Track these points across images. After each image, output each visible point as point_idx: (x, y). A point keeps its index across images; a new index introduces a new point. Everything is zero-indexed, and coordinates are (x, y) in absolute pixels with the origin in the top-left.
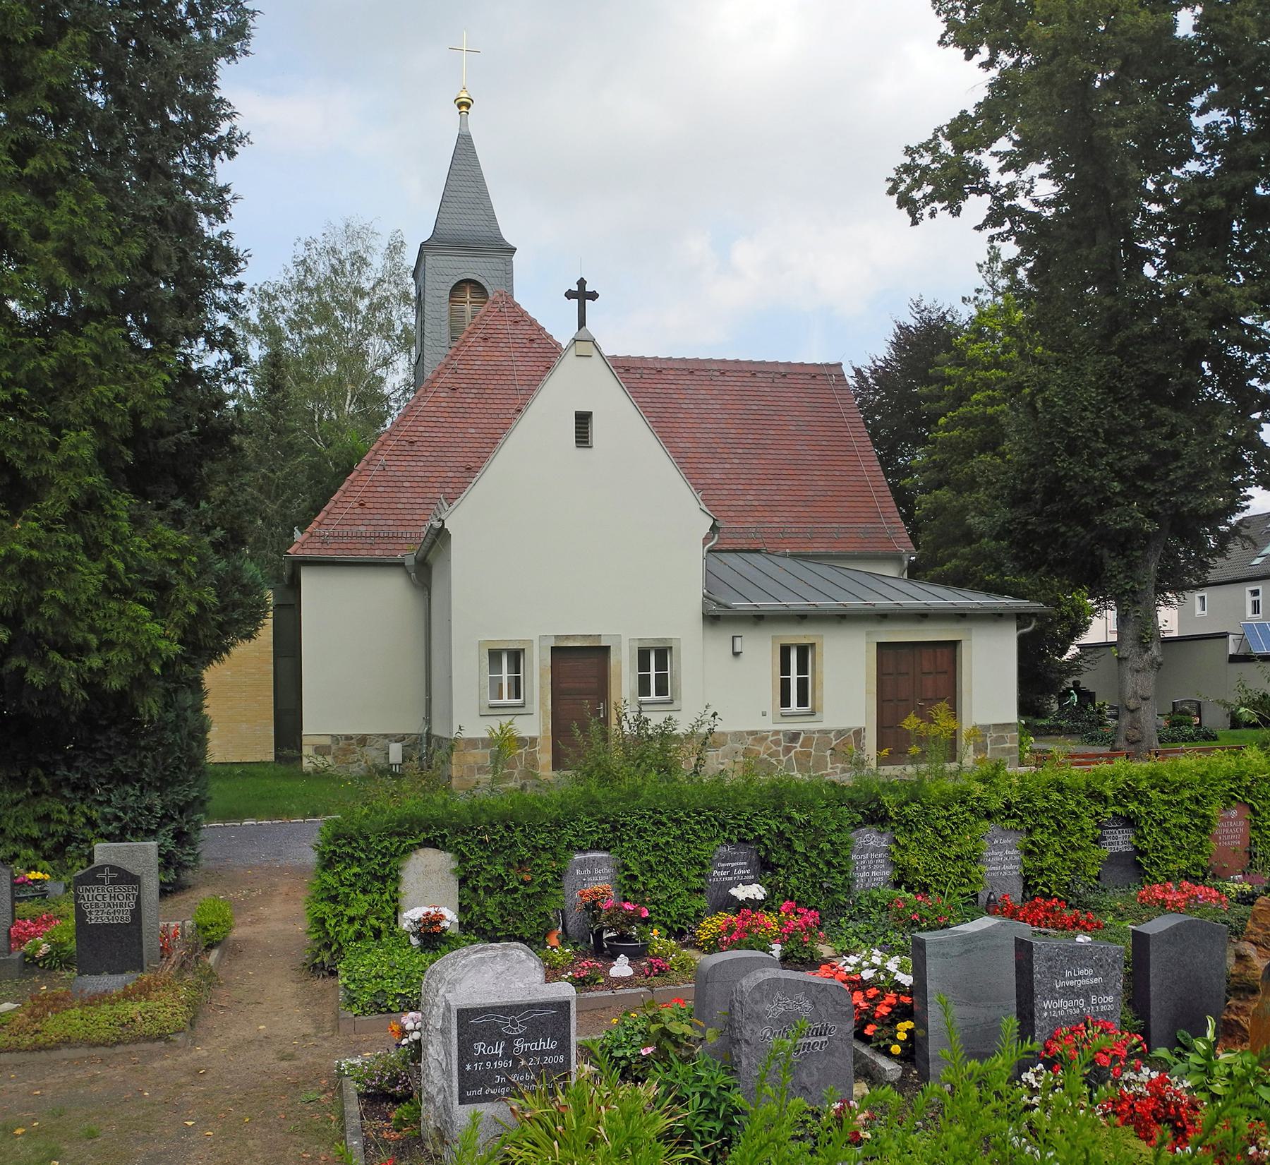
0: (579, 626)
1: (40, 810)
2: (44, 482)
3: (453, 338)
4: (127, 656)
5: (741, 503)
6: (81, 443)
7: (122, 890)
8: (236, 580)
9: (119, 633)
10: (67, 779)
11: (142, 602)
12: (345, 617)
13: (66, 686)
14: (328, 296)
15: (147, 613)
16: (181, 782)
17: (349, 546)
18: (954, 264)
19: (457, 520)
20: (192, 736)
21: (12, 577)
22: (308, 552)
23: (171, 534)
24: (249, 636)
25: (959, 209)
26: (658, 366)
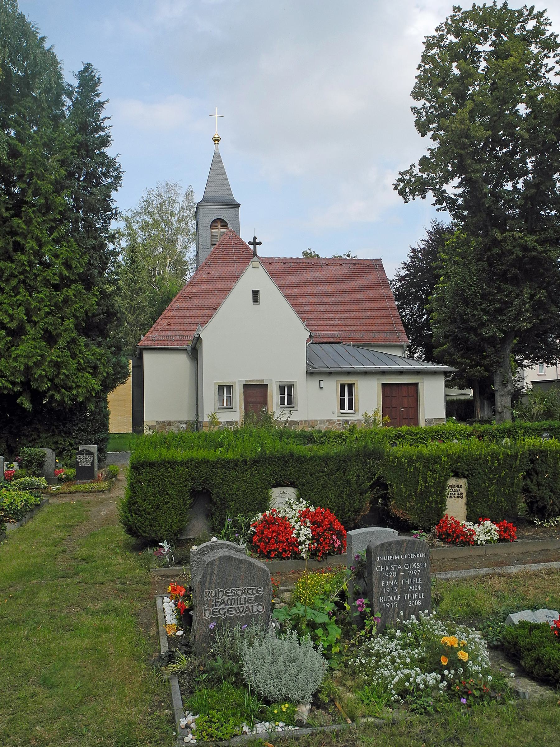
0: (255, 376)
1: (55, 440)
2: (59, 335)
3: (212, 244)
4: (84, 390)
5: (332, 322)
6: (70, 323)
7: (89, 457)
8: (119, 364)
9: (81, 382)
10: (63, 430)
11: (89, 372)
12: (162, 372)
13: (66, 400)
14: (159, 214)
15: (91, 376)
16: (101, 432)
17: (164, 342)
18: (426, 217)
19: (205, 334)
20: (104, 417)
21: (51, 367)
22: (146, 344)
23: (98, 350)
24: (123, 383)
25: (425, 196)
26: (298, 262)
